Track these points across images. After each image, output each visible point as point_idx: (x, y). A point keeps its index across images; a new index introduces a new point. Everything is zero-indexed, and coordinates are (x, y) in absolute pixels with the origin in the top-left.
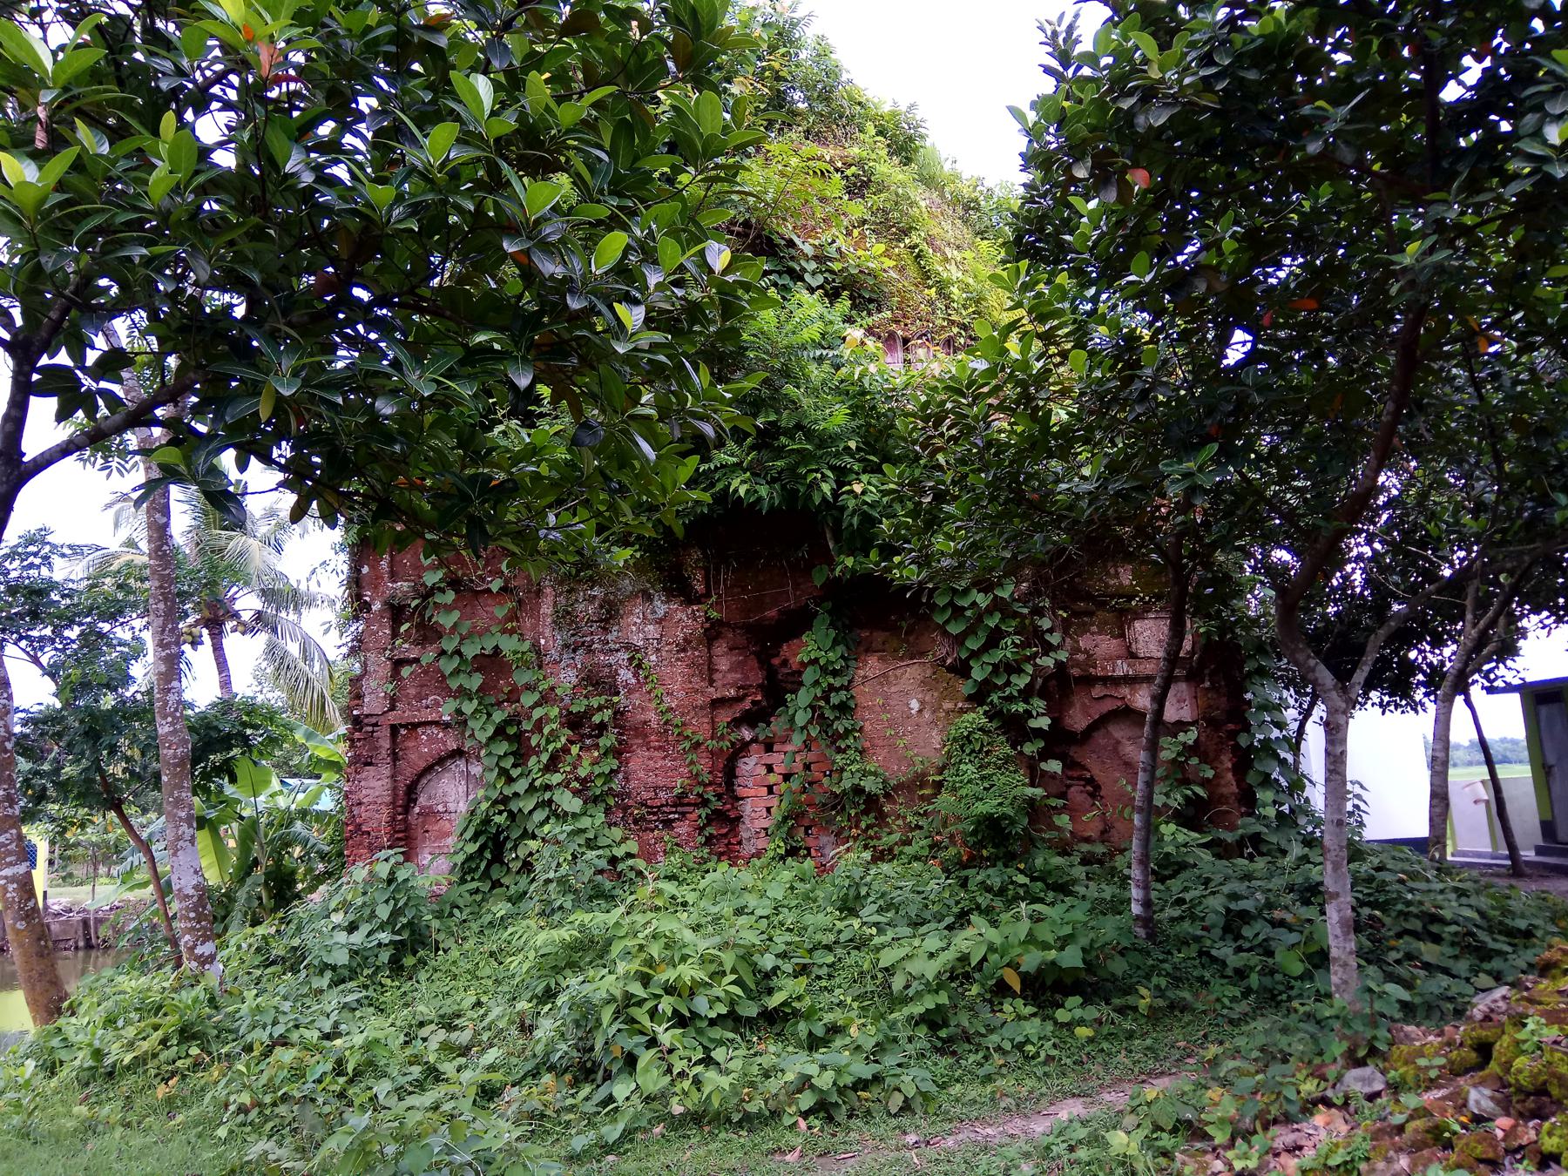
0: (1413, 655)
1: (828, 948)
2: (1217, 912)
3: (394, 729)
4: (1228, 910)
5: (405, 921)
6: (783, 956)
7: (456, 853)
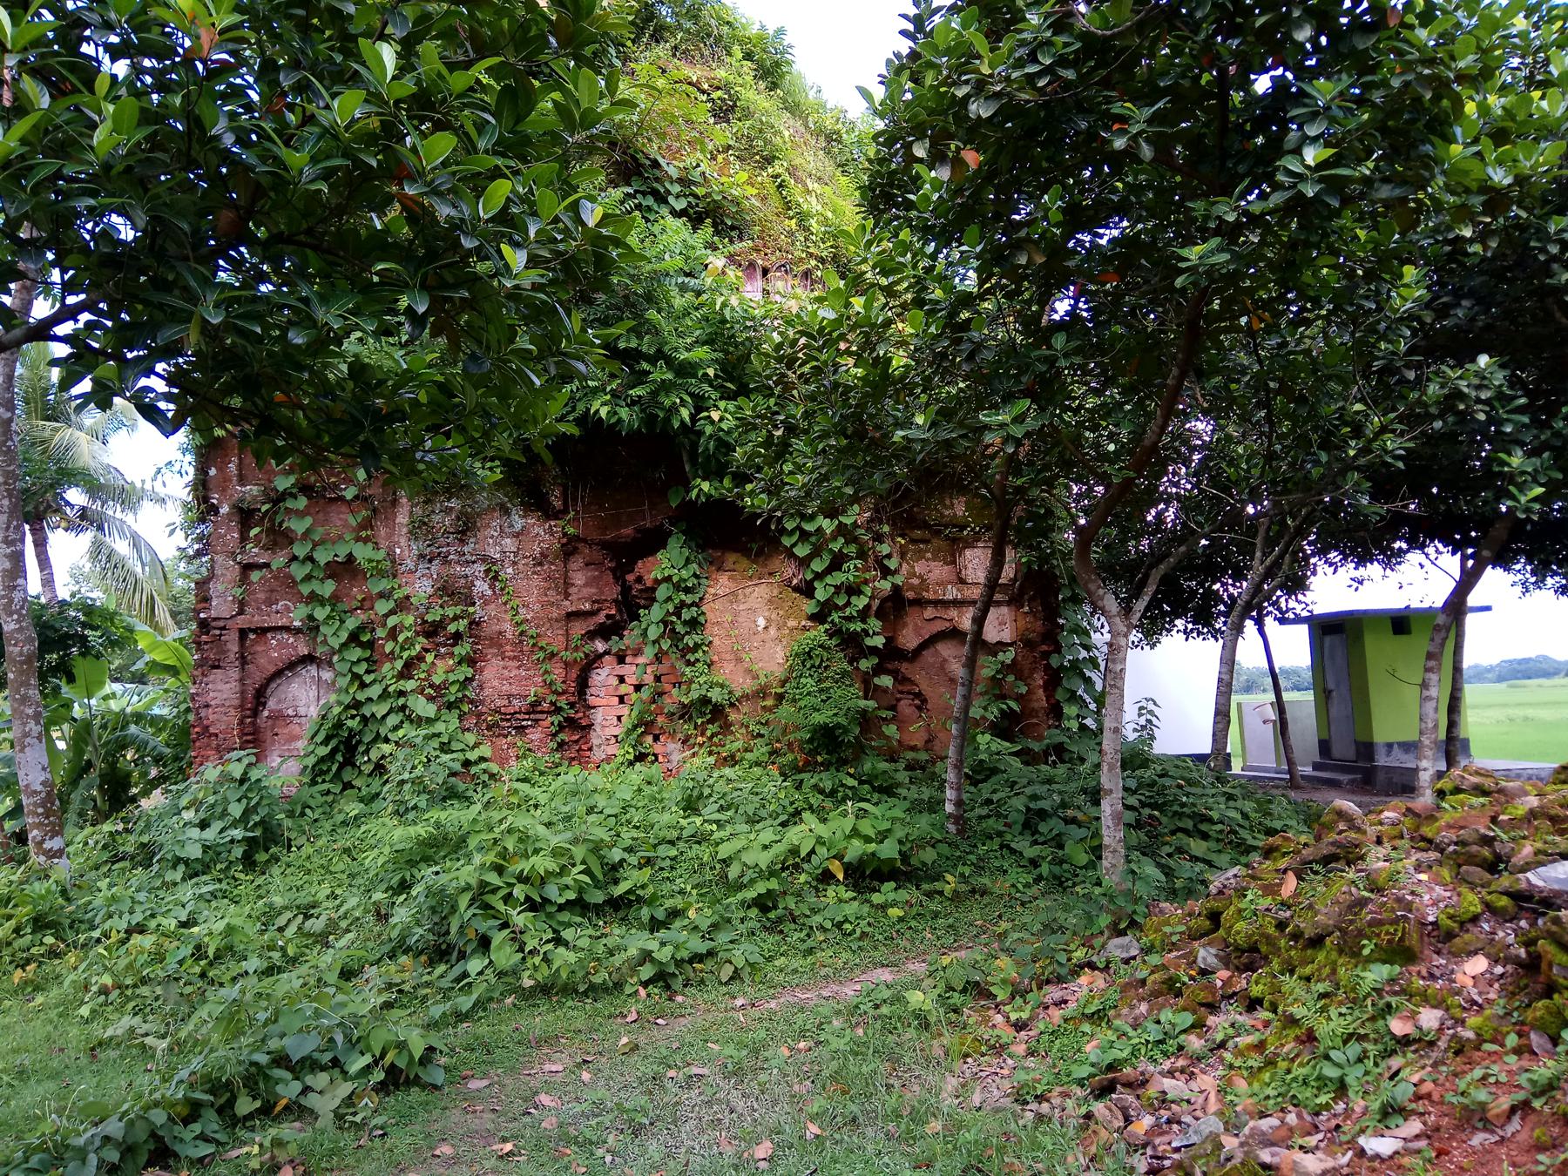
0: (1216, 587)
1: (672, 843)
2: (1018, 811)
3: (243, 633)
4: (1028, 809)
5: (257, 819)
6: (629, 850)
7: (307, 755)
